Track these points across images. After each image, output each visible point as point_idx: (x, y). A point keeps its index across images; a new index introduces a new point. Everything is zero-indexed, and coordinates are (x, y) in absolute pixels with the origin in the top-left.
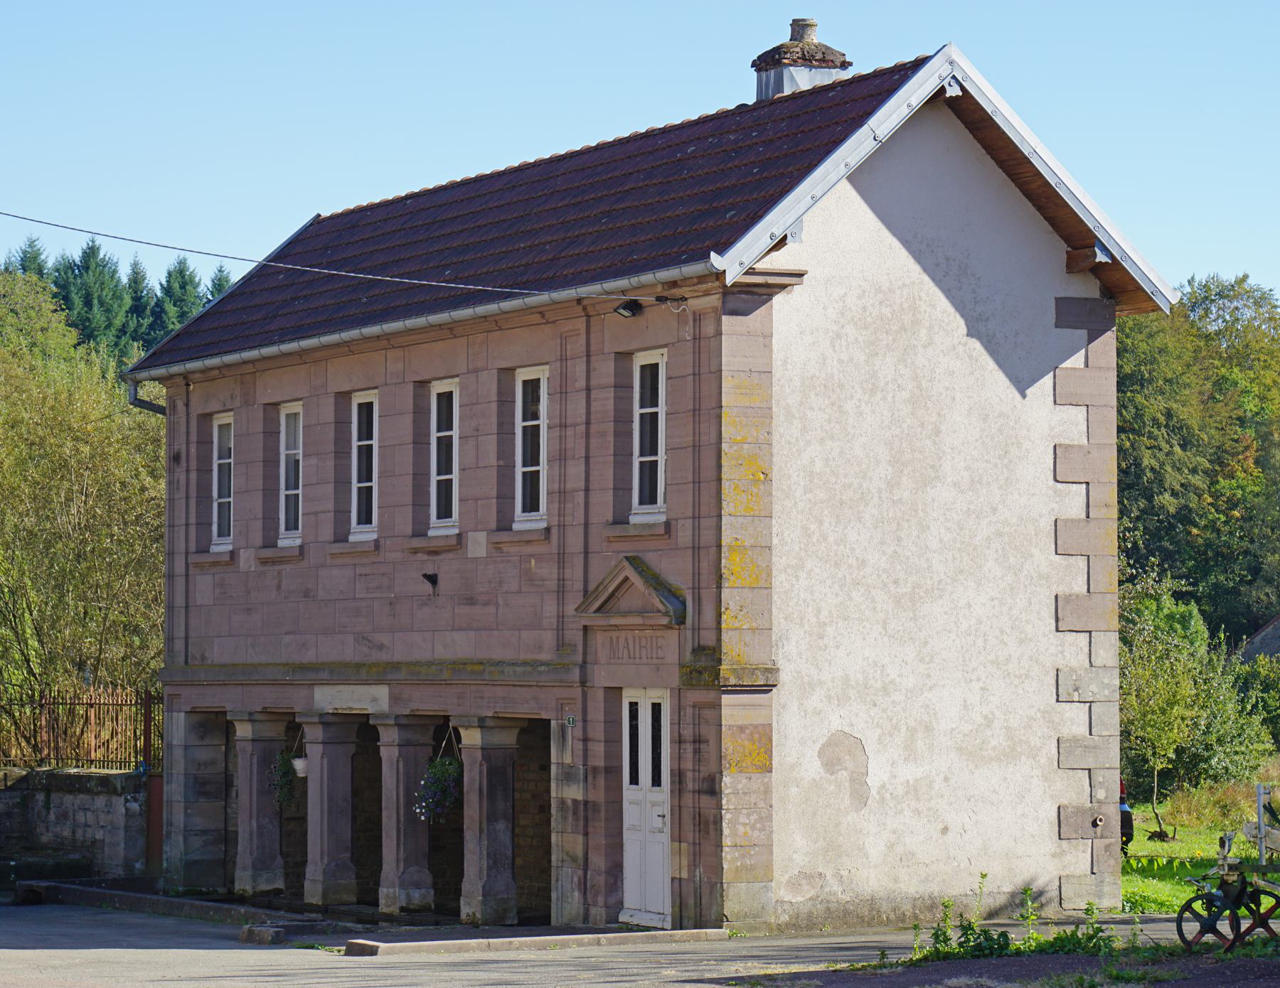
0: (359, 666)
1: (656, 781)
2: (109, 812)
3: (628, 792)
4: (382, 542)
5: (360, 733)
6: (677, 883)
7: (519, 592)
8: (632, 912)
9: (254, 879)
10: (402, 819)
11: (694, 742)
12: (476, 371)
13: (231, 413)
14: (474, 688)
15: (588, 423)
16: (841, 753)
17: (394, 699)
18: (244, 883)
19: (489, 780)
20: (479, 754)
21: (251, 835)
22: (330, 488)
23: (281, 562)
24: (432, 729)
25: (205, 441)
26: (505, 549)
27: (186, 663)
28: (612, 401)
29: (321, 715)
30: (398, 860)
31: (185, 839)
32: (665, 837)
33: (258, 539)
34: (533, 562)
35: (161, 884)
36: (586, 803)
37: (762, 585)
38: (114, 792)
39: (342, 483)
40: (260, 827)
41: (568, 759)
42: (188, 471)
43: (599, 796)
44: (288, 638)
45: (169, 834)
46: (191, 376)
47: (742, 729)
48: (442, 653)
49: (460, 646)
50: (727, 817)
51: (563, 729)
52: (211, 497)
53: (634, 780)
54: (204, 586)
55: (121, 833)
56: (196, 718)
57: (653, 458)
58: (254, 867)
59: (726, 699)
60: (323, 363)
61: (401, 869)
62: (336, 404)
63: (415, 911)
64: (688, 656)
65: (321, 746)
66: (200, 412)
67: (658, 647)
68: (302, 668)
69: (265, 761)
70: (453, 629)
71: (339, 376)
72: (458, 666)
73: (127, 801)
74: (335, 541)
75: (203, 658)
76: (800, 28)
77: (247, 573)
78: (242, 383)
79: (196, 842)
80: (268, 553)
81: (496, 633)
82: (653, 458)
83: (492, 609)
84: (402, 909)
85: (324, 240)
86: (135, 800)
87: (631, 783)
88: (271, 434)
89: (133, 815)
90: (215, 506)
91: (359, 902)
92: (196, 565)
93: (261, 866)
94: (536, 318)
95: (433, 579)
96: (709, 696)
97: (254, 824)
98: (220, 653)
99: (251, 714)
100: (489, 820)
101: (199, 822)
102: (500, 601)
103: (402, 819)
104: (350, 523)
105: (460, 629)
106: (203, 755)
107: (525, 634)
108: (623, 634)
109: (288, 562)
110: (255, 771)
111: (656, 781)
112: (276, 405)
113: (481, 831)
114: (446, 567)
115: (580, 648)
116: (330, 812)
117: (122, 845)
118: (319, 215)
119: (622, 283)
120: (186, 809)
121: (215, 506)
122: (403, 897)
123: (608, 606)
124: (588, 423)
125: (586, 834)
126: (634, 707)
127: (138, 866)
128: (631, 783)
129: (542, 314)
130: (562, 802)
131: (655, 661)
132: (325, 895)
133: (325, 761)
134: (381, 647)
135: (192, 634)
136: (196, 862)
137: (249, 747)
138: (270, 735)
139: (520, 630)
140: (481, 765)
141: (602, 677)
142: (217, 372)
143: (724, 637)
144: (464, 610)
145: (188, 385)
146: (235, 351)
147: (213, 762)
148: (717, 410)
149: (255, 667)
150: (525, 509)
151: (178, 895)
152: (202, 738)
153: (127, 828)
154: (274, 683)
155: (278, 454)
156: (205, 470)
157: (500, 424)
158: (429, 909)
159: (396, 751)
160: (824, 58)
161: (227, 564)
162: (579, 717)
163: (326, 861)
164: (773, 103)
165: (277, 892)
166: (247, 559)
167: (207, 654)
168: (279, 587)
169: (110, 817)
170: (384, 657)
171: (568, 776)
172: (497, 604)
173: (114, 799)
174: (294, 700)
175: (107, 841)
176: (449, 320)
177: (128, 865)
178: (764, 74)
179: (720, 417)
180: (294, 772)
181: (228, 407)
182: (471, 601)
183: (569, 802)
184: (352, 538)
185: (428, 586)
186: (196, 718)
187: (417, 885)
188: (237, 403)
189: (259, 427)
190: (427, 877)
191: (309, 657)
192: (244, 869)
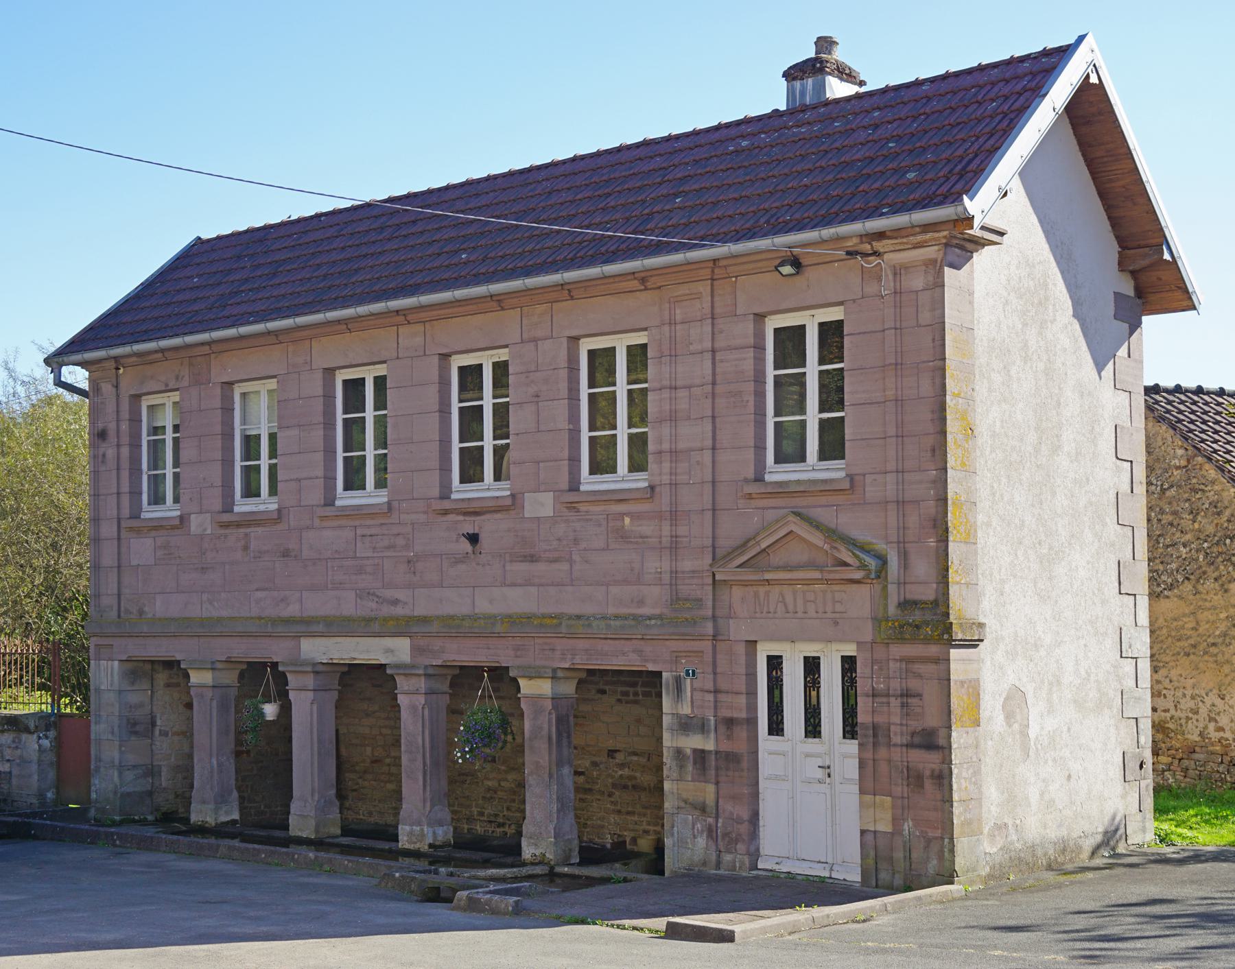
0: (368, 620)
1: (813, 728)
2: (17, 748)
3: (766, 742)
4: (395, 504)
5: (361, 685)
6: (870, 837)
7: (607, 549)
8: (777, 860)
9: (216, 811)
10: (428, 762)
11: (902, 696)
12: (535, 340)
13: (275, 380)
14: (537, 641)
15: (714, 383)
16: (1015, 701)
17: (416, 650)
18: (201, 814)
19: (557, 728)
20: (548, 705)
21: (212, 772)
22: (320, 456)
23: (249, 526)
24: (449, 678)
25: (135, 420)
26: (583, 507)
27: (119, 616)
28: (752, 361)
29: (314, 665)
30: (424, 801)
31: (120, 774)
32: (855, 789)
33: (217, 505)
34: (627, 520)
35: (92, 813)
36: (717, 752)
37: (970, 539)
38: (27, 730)
39: (228, 463)
40: (220, 765)
41: (686, 709)
42: (118, 446)
43: (740, 746)
44: (259, 594)
45: (97, 769)
46: (122, 361)
47: (962, 683)
48: (484, 606)
49: (519, 601)
50: (955, 771)
51: (678, 682)
52: (141, 470)
53: (776, 727)
54: (142, 550)
55: (34, 767)
56: (129, 666)
57: (479, 444)
58: (216, 803)
59: (954, 653)
60: (308, 342)
61: (428, 809)
62: (324, 378)
63: (440, 847)
64: (892, 610)
65: (310, 695)
66: (133, 392)
67: (834, 602)
68: (288, 621)
69: (223, 707)
70: (504, 584)
71: (325, 352)
72: (515, 621)
73: (40, 738)
74: (325, 505)
75: (141, 612)
76: (825, 44)
77: (202, 537)
78: (191, 364)
79: (129, 776)
80: (226, 517)
81: (570, 589)
82: (479, 444)
83: (565, 566)
84: (431, 846)
85: (199, 254)
86: (47, 737)
87: (770, 733)
88: (228, 410)
89: (45, 751)
90: (145, 478)
91: (342, 835)
92: (131, 529)
93: (221, 799)
94: (635, 284)
95: (474, 539)
96: (933, 650)
97: (214, 761)
98: (159, 608)
99: (213, 663)
100: (557, 765)
101: (131, 758)
102: (576, 557)
103: (428, 762)
104: (335, 489)
105: (514, 585)
106: (134, 698)
107: (614, 590)
108: (777, 589)
109: (259, 525)
110: (215, 714)
111: (813, 728)
112: (230, 384)
113: (551, 776)
114: (488, 527)
115: (710, 603)
116: (319, 754)
117: (36, 777)
118: (199, 238)
119: (782, 240)
120: (121, 746)
121: (145, 478)
122: (430, 835)
123: (753, 562)
124: (714, 383)
125: (717, 783)
126: (775, 663)
127: (49, 795)
128: (770, 733)
129: (643, 281)
130: (679, 752)
131: (829, 615)
132: (317, 831)
133: (315, 707)
134: (395, 602)
135: (125, 591)
136: (129, 794)
137: (209, 693)
138: (227, 682)
139: (608, 585)
140: (550, 713)
141: (739, 631)
142: (160, 355)
143: (953, 590)
144: (524, 567)
145: (118, 369)
146: (177, 335)
147: (141, 705)
148: (939, 363)
149: (219, 620)
150: (463, 480)
151: (114, 824)
152: (133, 683)
153: (40, 762)
154: (242, 635)
155: (233, 429)
156: (135, 446)
157: (570, 390)
158: (450, 845)
159: (422, 699)
160: (846, 74)
161: (173, 528)
162: (710, 669)
163: (316, 798)
164: (804, 109)
165: (234, 822)
166: (200, 524)
167: (146, 609)
168: (246, 548)
169: (19, 752)
170: (399, 611)
171: (685, 725)
172: (571, 562)
173: (24, 736)
174: (275, 651)
175: (15, 772)
176: (417, 304)
177: (41, 795)
178: (798, 84)
179: (944, 369)
180: (262, 715)
181: (171, 386)
182: (532, 559)
183: (688, 752)
184: (338, 503)
185: (466, 546)
186: (129, 666)
187: (441, 823)
188: (185, 383)
189: (217, 403)
190: (446, 815)
191: (292, 610)
192: (204, 802)
